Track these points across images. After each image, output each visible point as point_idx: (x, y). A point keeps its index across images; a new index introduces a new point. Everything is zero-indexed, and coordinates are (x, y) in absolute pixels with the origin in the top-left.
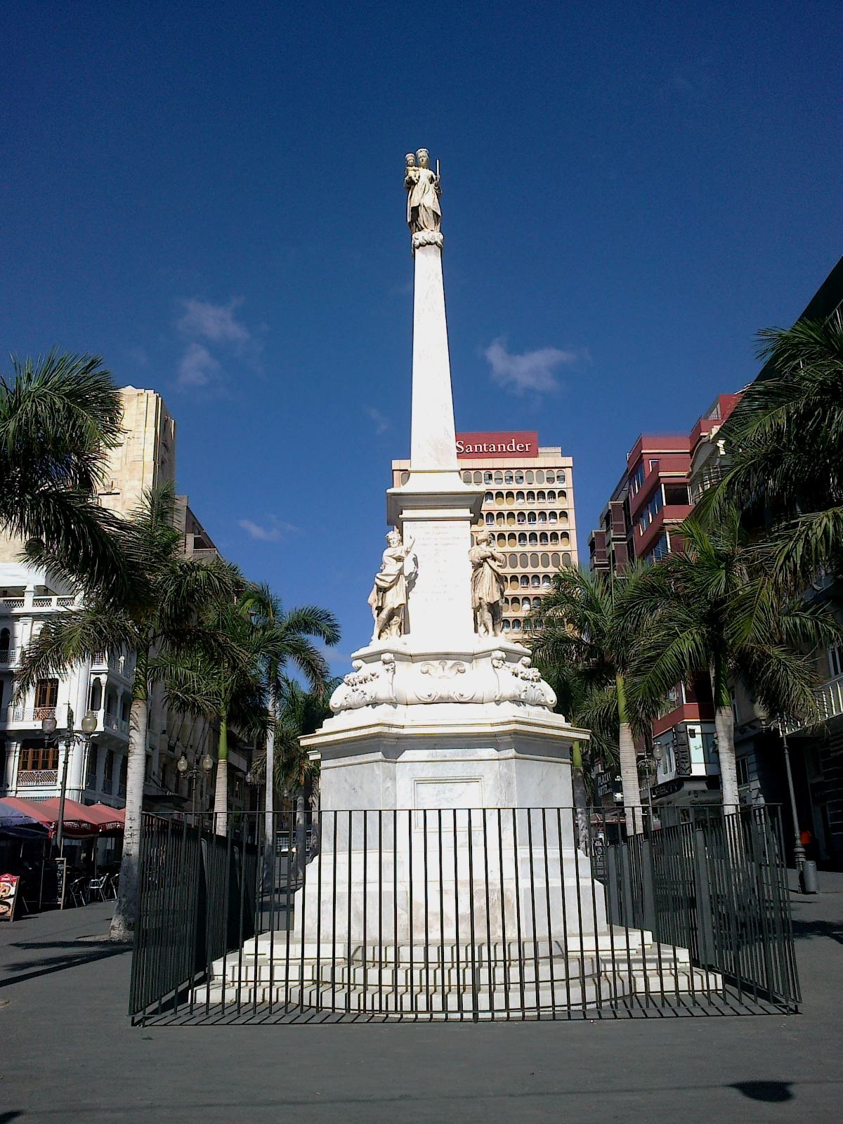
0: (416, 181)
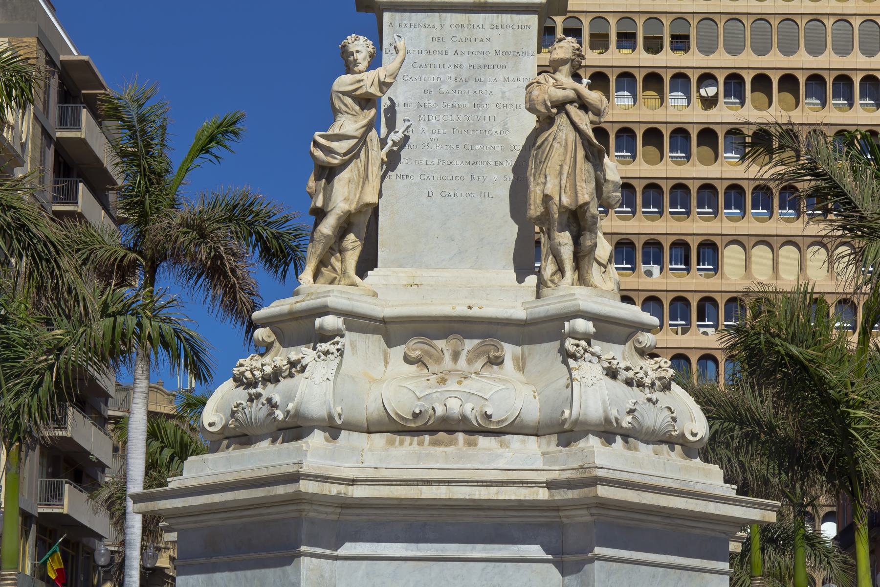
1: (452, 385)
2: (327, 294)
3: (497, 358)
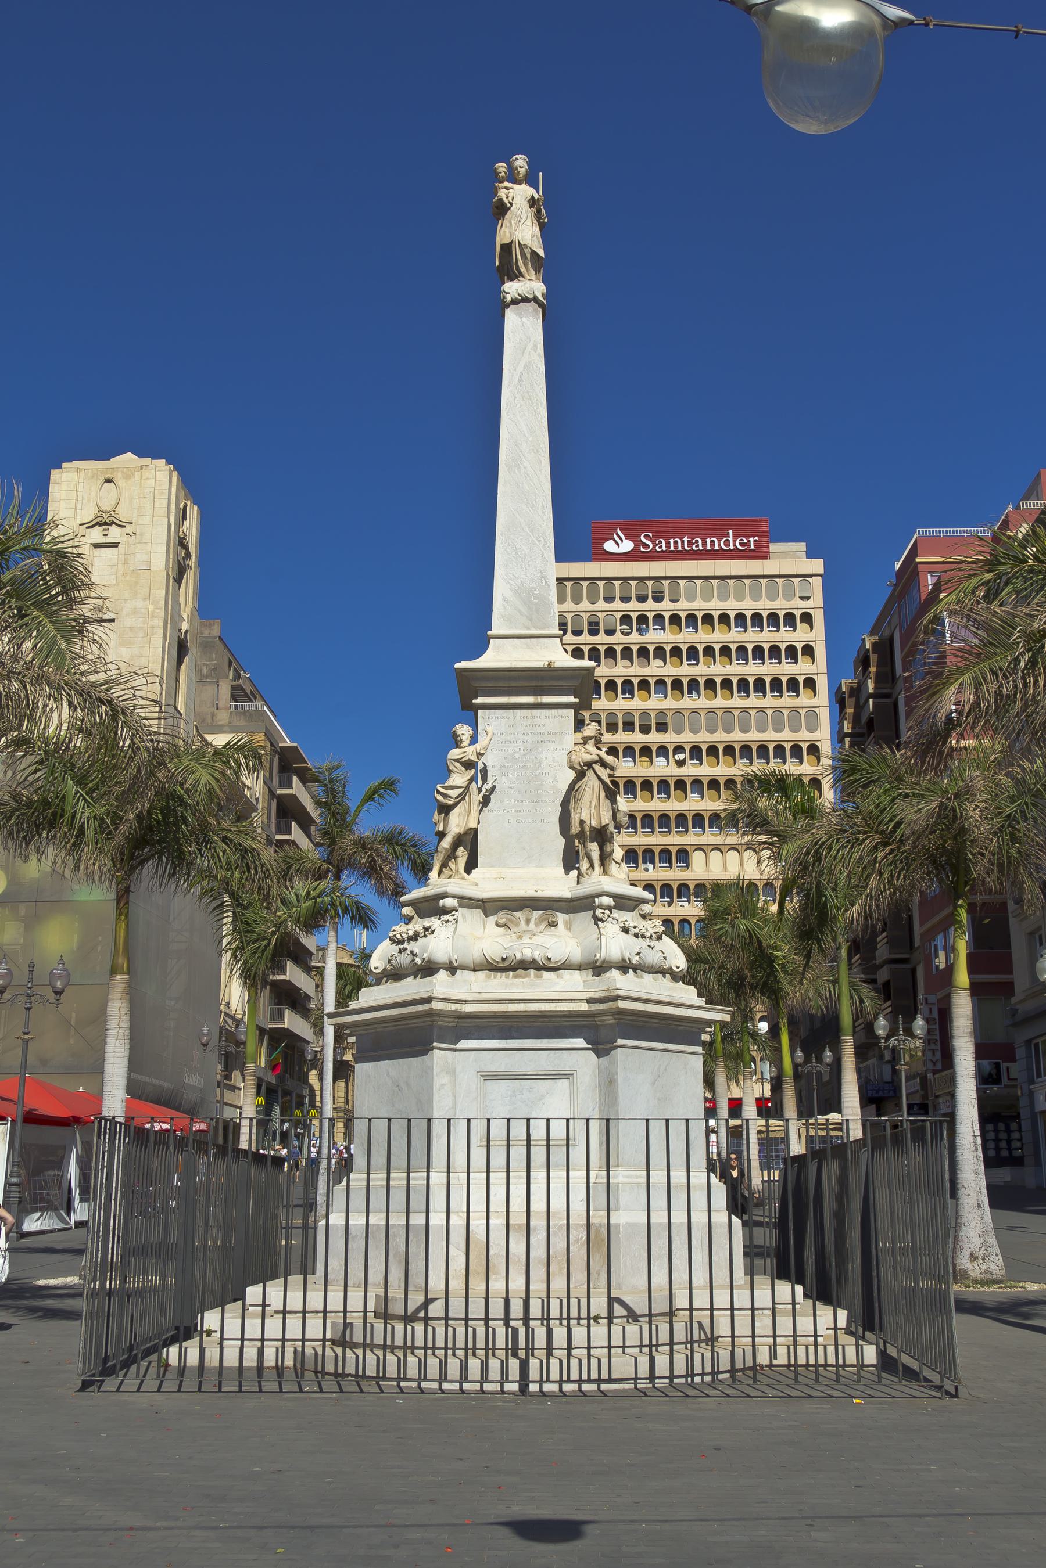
0: (509, 205)
1: (526, 940)
2: (447, 884)
3: (554, 922)
